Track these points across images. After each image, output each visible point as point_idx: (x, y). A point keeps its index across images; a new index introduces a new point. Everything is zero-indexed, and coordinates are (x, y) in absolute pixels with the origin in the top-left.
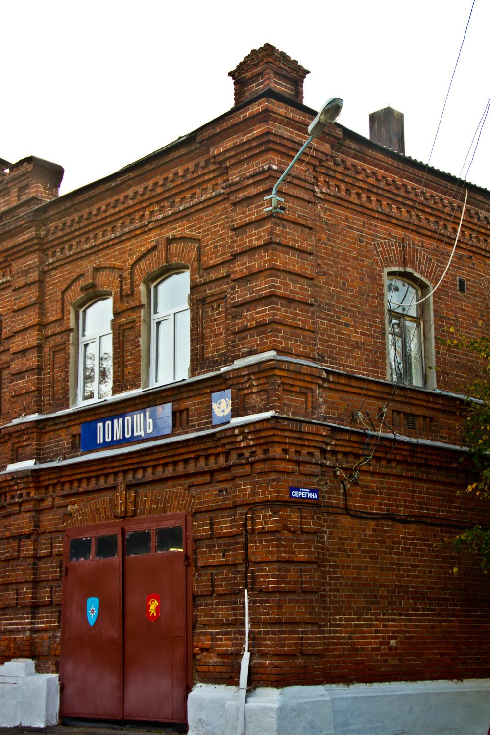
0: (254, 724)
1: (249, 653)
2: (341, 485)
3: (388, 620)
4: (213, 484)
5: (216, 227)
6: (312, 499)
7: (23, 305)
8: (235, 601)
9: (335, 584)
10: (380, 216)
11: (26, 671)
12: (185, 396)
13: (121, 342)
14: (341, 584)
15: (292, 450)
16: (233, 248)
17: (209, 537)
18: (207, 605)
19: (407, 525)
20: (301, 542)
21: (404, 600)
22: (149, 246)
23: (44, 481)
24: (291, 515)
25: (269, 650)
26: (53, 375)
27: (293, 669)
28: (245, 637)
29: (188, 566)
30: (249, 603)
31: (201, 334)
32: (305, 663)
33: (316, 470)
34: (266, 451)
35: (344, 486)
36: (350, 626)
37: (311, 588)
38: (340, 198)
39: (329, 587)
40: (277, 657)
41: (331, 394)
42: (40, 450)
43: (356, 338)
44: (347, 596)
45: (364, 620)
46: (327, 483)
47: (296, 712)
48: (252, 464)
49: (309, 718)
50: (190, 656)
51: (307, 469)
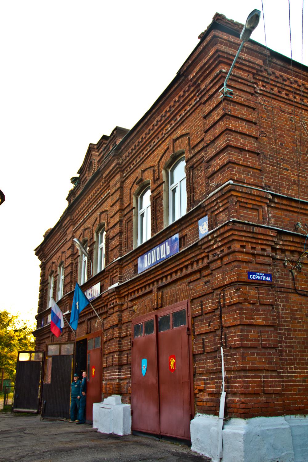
0: (229, 445)
1: (225, 393)
2: (290, 273)
4: (202, 279)
5: (197, 122)
6: (267, 281)
7: (114, 202)
8: (215, 356)
9: (290, 343)
11: (116, 402)
12: (184, 226)
13: (155, 206)
14: (294, 342)
15: (249, 246)
16: (205, 127)
17: (200, 314)
18: (201, 360)
20: (259, 311)
22: (166, 148)
23: (122, 293)
26: (127, 235)
27: (257, 405)
28: (222, 381)
29: (189, 335)
31: (192, 187)
33: (269, 261)
34: (229, 248)
35: (292, 273)
37: (269, 344)
39: (284, 344)
40: (243, 396)
41: (278, 212)
44: (299, 351)
46: (278, 272)
47: (260, 437)
49: (272, 441)
51: (261, 259)
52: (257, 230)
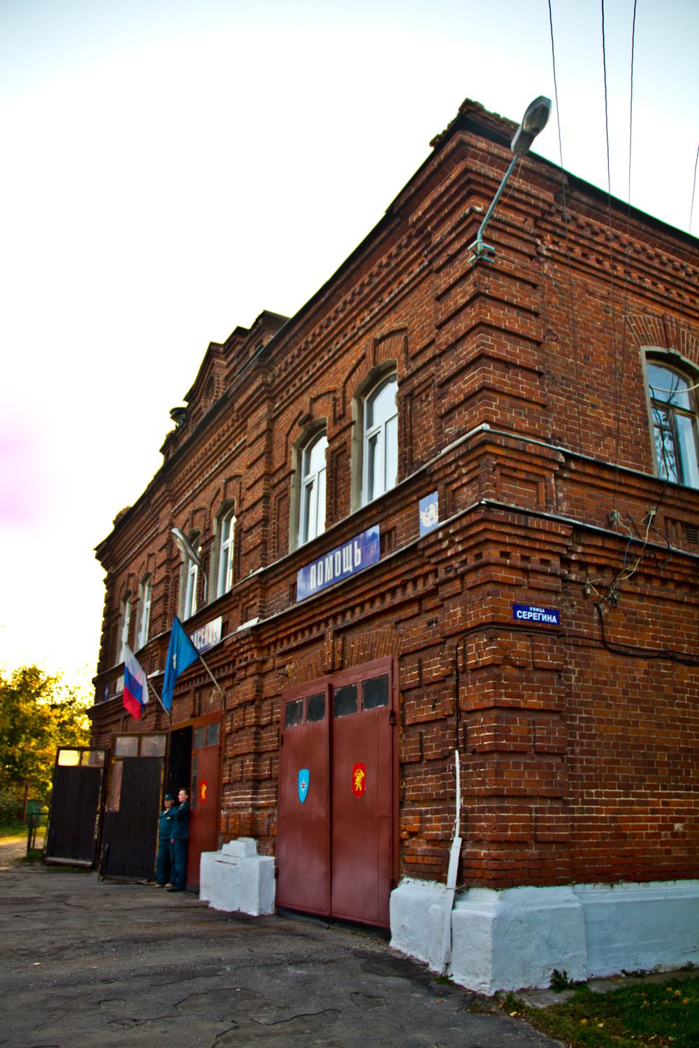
1: (461, 839)
2: (595, 609)
3: (670, 796)
4: (422, 615)
6: (549, 623)
9: (589, 745)
10: (631, 287)
14: (598, 745)
15: (517, 554)
19: (694, 668)
20: (533, 682)
21: (693, 768)
22: (360, 356)
23: (265, 639)
24: (516, 643)
25: (484, 835)
29: (394, 725)
30: (461, 769)
32: (539, 853)
34: (479, 556)
35: (599, 611)
36: (614, 803)
37: (548, 747)
38: (573, 259)
39: (579, 748)
40: (495, 846)
41: (575, 488)
42: (265, 607)
43: (608, 422)
44: (606, 762)
45: (635, 795)
46: (573, 606)
48: (462, 577)
50: (397, 842)
51: (541, 581)
52: (533, 522)
